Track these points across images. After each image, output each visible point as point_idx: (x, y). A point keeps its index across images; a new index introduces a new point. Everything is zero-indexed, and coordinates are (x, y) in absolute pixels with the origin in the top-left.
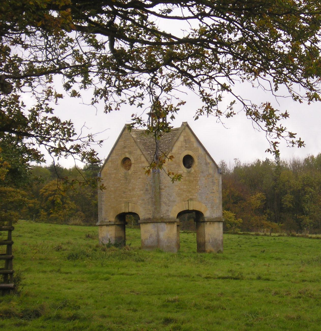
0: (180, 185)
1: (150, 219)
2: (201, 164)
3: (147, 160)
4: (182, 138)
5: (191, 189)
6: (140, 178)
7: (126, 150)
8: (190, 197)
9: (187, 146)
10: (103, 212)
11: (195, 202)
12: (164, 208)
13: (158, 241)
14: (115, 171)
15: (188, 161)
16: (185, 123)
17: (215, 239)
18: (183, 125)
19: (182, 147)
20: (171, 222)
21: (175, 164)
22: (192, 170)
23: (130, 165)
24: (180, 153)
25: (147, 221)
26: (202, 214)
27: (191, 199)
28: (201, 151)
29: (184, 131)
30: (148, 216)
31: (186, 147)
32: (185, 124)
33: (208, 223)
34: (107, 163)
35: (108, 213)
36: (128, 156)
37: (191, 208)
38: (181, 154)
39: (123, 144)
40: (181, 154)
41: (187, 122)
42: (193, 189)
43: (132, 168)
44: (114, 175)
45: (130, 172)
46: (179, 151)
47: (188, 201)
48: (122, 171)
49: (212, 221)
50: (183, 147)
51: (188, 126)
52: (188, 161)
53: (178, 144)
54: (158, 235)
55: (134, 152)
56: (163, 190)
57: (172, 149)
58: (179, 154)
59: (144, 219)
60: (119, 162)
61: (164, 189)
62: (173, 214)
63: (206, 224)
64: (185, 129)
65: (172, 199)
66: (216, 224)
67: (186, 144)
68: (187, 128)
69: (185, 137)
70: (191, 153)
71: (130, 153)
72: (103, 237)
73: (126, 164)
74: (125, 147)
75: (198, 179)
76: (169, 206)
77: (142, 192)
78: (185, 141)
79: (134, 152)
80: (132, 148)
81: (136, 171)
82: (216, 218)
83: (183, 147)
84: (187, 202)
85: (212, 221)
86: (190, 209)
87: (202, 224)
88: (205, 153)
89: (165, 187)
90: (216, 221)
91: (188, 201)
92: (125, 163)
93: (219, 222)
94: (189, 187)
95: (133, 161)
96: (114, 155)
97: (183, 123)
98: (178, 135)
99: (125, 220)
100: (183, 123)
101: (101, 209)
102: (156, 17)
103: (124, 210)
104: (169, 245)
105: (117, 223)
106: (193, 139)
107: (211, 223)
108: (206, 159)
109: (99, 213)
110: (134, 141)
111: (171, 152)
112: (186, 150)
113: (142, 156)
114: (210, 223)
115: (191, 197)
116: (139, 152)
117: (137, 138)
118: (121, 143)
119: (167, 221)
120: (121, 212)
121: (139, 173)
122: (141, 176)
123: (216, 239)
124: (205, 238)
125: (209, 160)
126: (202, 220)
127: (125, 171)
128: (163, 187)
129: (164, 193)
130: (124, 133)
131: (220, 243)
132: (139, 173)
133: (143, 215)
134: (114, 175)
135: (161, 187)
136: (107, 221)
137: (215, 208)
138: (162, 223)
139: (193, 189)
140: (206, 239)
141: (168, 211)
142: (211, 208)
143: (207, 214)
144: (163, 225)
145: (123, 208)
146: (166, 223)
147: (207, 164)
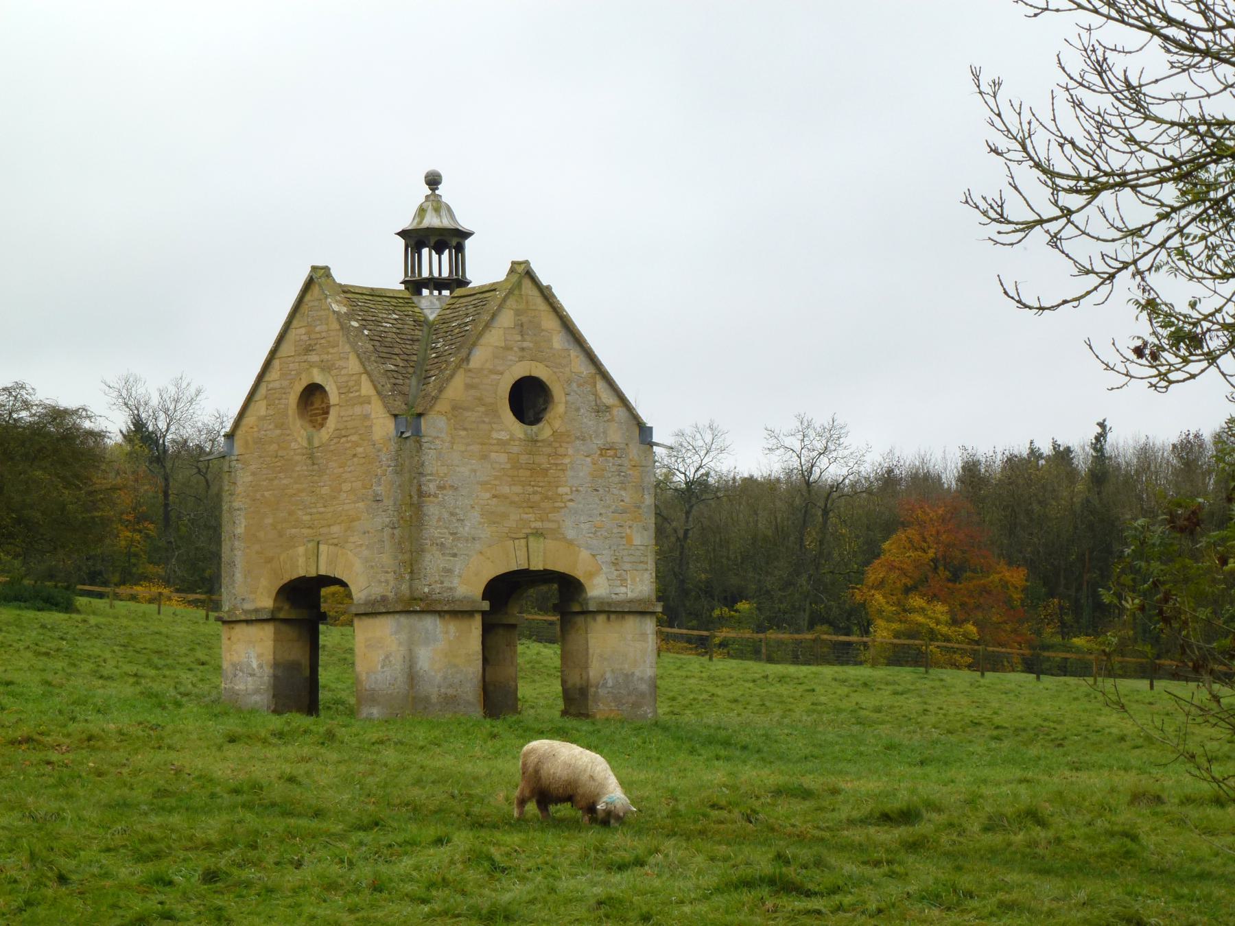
0: (497, 482)
1: (384, 599)
2: (578, 409)
3: (379, 393)
4: (506, 319)
5: (537, 498)
6: (355, 455)
7: (314, 358)
8: (533, 525)
9: (525, 344)
10: (239, 576)
11: (550, 544)
12: (433, 562)
13: (412, 676)
14: (278, 432)
15: (528, 399)
16: (519, 263)
17: (627, 675)
18: (512, 271)
19: (508, 348)
20: (458, 613)
21: (482, 409)
22: (544, 430)
23: (326, 412)
24: (500, 368)
25: (375, 610)
26: (579, 582)
27: (539, 534)
28: (580, 366)
29: (516, 292)
30: (377, 591)
31: (523, 349)
32: (520, 269)
33: (601, 618)
34: (252, 404)
35: (251, 584)
36: (318, 378)
37: (537, 565)
38: (502, 374)
39: (305, 338)
40: (502, 374)
41: (527, 262)
42: (547, 498)
43: (332, 421)
44: (274, 447)
45: (324, 434)
46: (496, 361)
47: (527, 538)
48: (299, 431)
49: (615, 611)
50: (511, 349)
51: (530, 275)
52: (528, 399)
53: (493, 338)
54: (411, 662)
55: (341, 363)
56: (432, 499)
57: (469, 354)
58: (492, 372)
59: (367, 603)
60: (293, 398)
61: (436, 496)
62: (468, 580)
63: (595, 620)
64: (519, 285)
65: (465, 531)
66: (631, 624)
67: (524, 340)
68: (527, 283)
69: (518, 313)
70: (540, 372)
71: (326, 368)
72: (234, 665)
73: (316, 406)
74: (308, 350)
75: (567, 461)
76: (455, 555)
77: (361, 505)
78: (520, 327)
79: (338, 363)
80: (331, 350)
81: (343, 432)
82: (631, 601)
83: (511, 349)
84: (523, 542)
85: (615, 611)
86: (532, 568)
87: (580, 620)
88: (592, 370)
89: (441, 488)
90: (629, 613)
91: (527, 538)
92: (312, 404)
93: (643, 613)
94: (531, 490)
95: (333, 397)
96: (273, 375)
97: (513, 263)
98: (493, 306)
99: (306, 604)
100: (513, 263)
101: (232, 564)
102: (323, 658)
103: (303, 568)
104: (451, 692)
105: (282, 615)
106: (550, 323)
107: (613, 617)
108: (595, 394)
109: (225, 580)
110: (338, 327)
111: (464, 366)
112: (522, 359)
113: (364, 377)
114: (609, 619)
115: (539, 524)
116: (353, 365)
117: (350, 316)
118: (296, 333)
119: (446, 608)
120: (295, 576)
121: (354, 438)
122: (360, 450)
123: (628, 677)
124: (586, 667)
125: (607, 398)
126: (576, 608)
127: (310, 429)
128: (432, 487)
129: (432, 510)
130: (308, 297)
131: (644, 687)
132: (354, 438)
133: (362, 587)
134: (274, 447)
135: (424, 488)
136: (247, 606)
137: (627, 566)
138: (424, 616)
139: (547, 498)
140: (591, 674)
141: (448, 571)
142: (618, 568)
143: (598, 588)
144: (430, 624)
145: (301, 561)
146: (440, 613)
147: (601, 410)
